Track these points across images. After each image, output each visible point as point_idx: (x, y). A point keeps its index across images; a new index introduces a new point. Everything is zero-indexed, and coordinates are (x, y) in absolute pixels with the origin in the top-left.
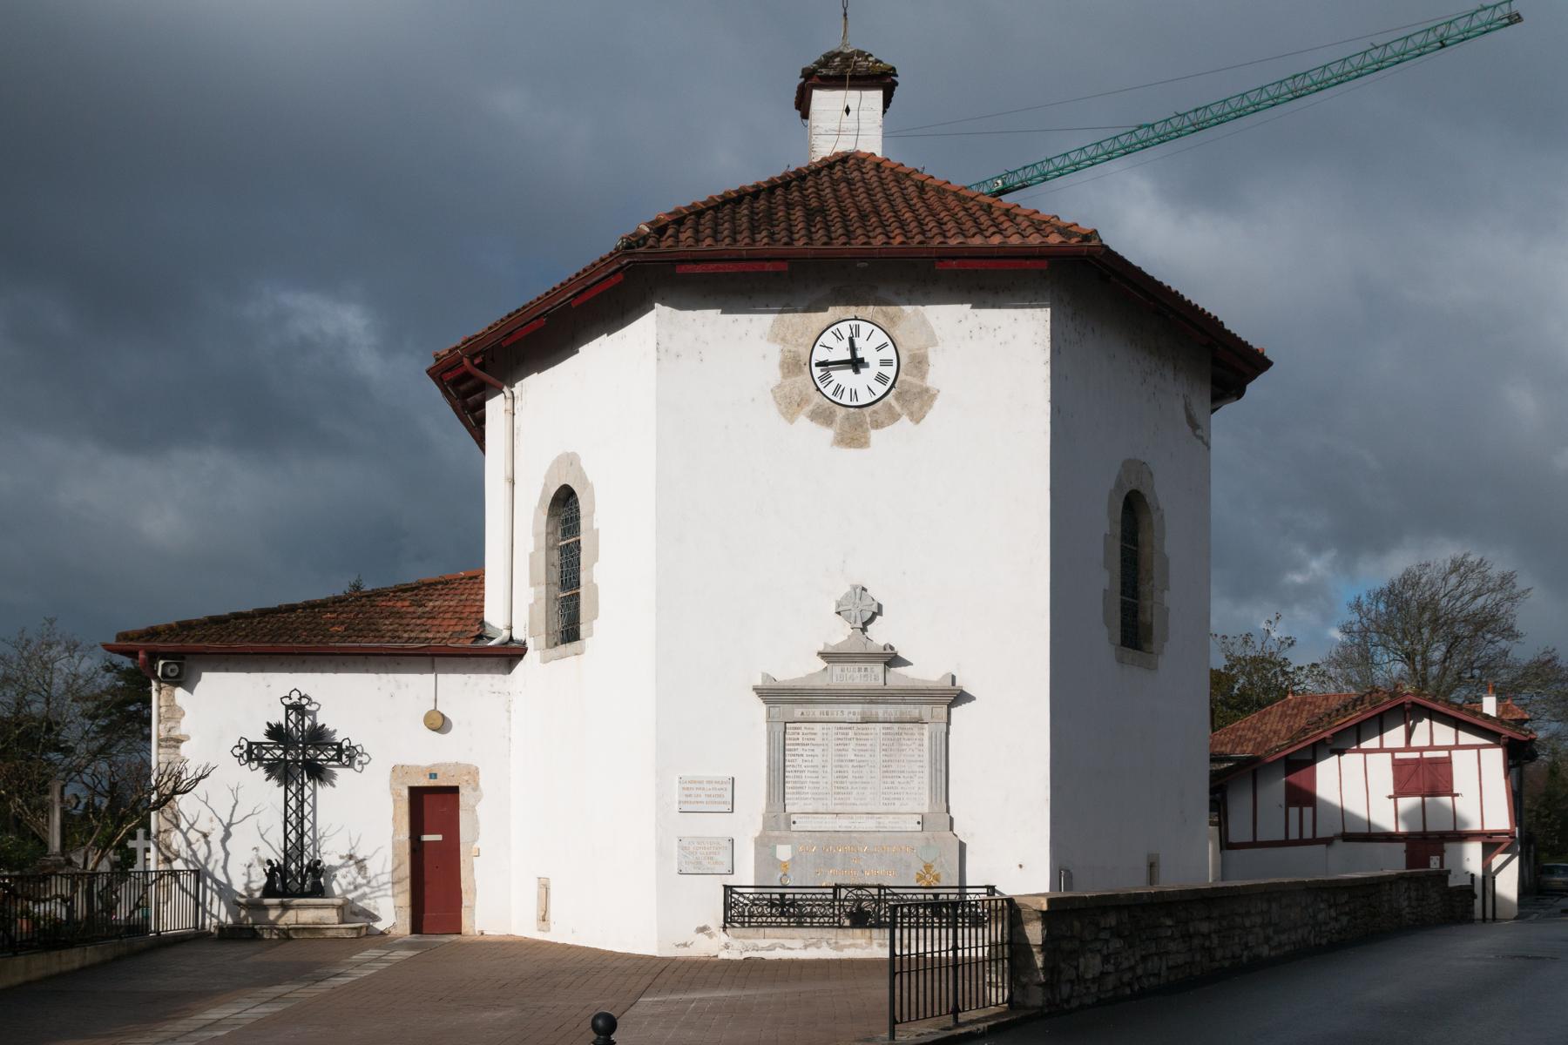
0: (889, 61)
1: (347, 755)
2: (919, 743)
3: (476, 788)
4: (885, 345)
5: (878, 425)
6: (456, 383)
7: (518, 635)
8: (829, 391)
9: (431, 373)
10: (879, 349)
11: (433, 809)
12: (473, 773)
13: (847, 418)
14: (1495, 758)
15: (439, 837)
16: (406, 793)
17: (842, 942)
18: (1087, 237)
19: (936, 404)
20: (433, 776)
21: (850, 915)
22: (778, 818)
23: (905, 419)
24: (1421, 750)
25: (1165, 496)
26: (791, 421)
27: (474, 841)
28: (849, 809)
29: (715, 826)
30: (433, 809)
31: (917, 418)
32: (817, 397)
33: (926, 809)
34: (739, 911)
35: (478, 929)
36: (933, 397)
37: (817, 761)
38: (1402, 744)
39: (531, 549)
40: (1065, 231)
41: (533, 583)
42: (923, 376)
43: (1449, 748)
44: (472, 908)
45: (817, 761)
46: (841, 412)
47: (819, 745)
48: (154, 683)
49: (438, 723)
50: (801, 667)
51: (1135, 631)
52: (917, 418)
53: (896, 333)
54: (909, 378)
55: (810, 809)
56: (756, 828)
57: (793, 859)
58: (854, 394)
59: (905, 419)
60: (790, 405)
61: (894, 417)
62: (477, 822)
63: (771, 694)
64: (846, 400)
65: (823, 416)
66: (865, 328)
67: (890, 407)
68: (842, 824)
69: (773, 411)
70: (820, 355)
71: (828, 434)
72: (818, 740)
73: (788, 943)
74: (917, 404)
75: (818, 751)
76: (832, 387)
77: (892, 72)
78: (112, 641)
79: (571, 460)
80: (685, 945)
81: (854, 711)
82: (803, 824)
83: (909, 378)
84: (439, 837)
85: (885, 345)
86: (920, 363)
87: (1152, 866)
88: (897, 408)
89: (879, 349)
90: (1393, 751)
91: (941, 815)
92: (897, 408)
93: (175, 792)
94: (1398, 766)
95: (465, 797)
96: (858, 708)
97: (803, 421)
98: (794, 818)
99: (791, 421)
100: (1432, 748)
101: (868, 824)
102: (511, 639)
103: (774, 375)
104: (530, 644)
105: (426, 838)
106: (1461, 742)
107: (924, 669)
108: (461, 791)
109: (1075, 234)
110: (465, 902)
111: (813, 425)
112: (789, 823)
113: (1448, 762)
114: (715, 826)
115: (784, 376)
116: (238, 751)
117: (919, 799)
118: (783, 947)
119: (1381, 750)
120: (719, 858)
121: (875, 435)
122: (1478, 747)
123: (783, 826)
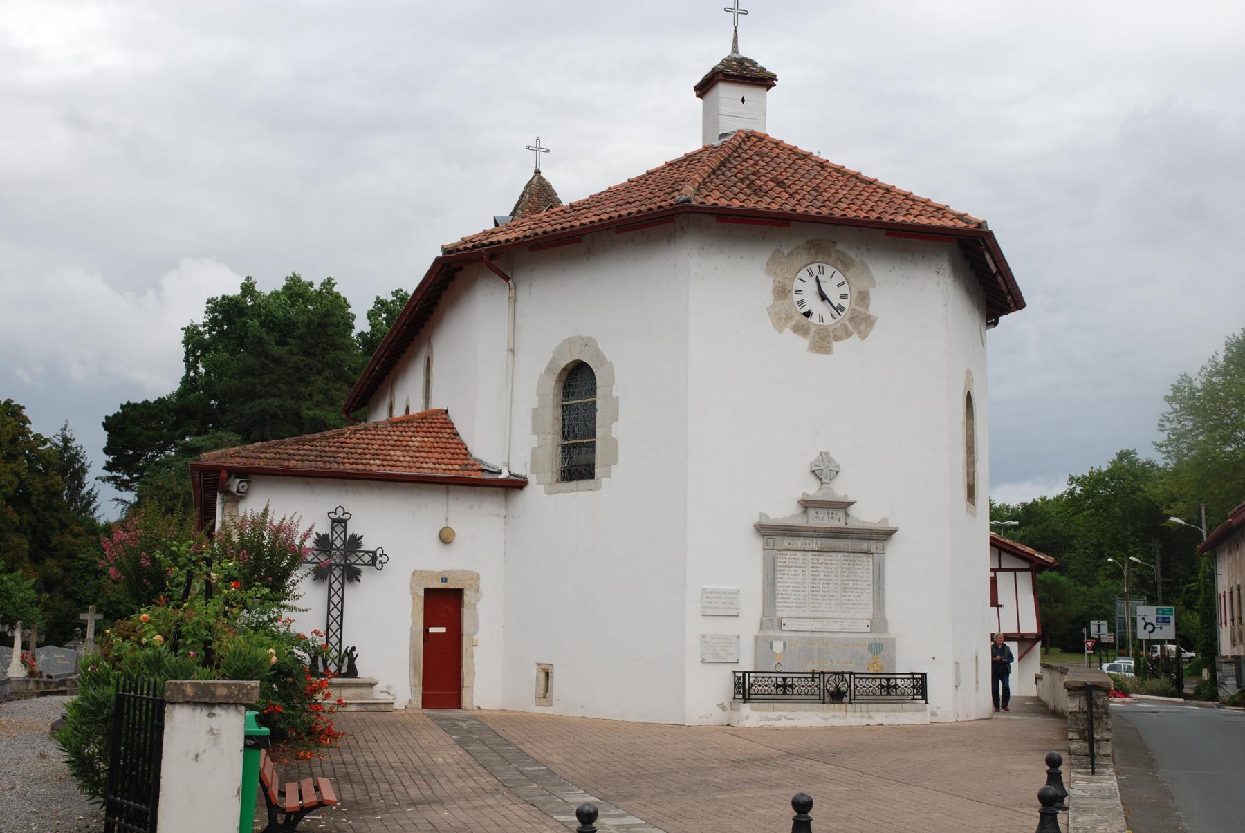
2: (864, 565)
3: (477, 590)
10: (839, 285)
11: (444, 604)
12: (475, 577)
14: (1025, 581)
15: (443, 630)
16: (422, 593)
18: (980, 225)
19: (875, 327)
20: (444, 580)
22: (771, 620)
23: (855, 335)
27: (475, 633)
28: (820, 615)
29: (725, 627)
30: (444, 604)
31: (863, 336)
34: (743, 689)
35: (476, 703)
36: (873, 322)
37: (799, 579)
39: (534, 402)
40: (962, 217)
41: (536, 430)
42: (867, 308)
44: (471, 687)
47: (799, 568)
48: (219, 496)
50: (784, 511)
52: (863, 336)
55: (794, 614)
56: (754, 629)
59: (855, 335)
61: (848, 334)
62: (477, 618)
63: (767, 531)
66: (829, 270)
68: (817, 625)
73: (790, 715)
74: (863, 327)
75: (799, 571)
81: (814, 544)
82: (790, 625)
84: (443, 630)
88: (850, 328)
89: (839, 285)
91: (878, 622)
95: (468, 597)
101: (835, 626)
104: (532, 479)
105: (432, 630)
107: (865, 515)
109: (795, 154)
111: (795, 335)
112: (781, 625)
114: (725, 627)
116: (384, 559)
117: (865, 611)
123: (776, 627)
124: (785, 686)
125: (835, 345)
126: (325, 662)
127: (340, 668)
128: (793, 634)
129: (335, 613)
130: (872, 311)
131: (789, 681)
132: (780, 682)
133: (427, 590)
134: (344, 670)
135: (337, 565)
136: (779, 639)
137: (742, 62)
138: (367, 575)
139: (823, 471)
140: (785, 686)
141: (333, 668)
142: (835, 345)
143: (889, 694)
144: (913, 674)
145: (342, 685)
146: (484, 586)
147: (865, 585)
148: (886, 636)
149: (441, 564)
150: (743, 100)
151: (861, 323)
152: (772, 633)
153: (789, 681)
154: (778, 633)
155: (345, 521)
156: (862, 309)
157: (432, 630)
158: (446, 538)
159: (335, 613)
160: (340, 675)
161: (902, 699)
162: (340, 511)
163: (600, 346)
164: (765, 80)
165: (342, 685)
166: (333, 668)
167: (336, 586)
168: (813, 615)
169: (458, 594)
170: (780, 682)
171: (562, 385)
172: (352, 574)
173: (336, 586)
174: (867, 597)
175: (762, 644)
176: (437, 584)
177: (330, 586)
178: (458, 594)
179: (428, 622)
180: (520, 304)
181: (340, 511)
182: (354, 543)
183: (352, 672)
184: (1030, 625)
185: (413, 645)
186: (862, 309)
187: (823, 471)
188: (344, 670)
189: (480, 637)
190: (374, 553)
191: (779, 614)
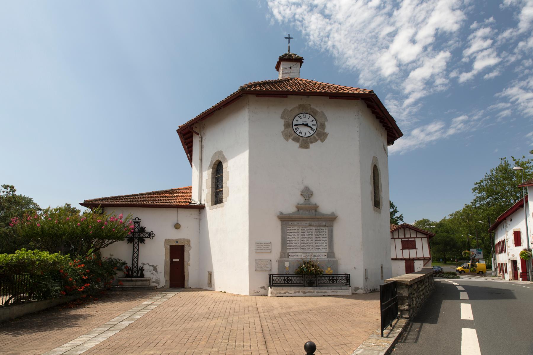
0: (301, 56)
1: (150, 235)
2: (326, 230)
3: (189, 246)
4: (313, 121)
5: (312, 142)
6: (184, 135)
7: (203, 203)
8: (298, 133)
9: (178, 131)
10: (312, 121)
12: (189, 241)
13: (303, 140)
14: (425, 241)
15: (178, 260)
16: (169, 247)
17: (306, 291)
19: (328, 137)
20: (177, 242)
21: (308, 283)
22: (284, 254)
23: (319, 141)
24: (408, 238)
25: (380, 167)
26: (287, 141)
29: (266, 257)
31: (323, 141)
32: (294, 134)
33: (327, 251)
37: (296, 237)
38: (403, 237)
43: (415, 238)
45: (296, 237)
46: (301, 139)
47: (295, 234)
49: (177, 226)
50: (290, 209)
51: (377, 204)
52: (323, 141)
53: (316, 117)
54: (320, 130)
57: (289, 266)
58: (305, 134)
59: (319, 141)
60: (287, 136)
61: (316, 141)
64: (303, 135)
65: (296, 139)
67: (315, 138)
69: (282, 138)
70: (295, 122)
71: (298, 145)
72: (296, 231)
74: (322, 137)
75: (296, 234)
76: (299, 131)
77: (302, 59)
78: (83, 202)
79: (220, 153)
80: (257, 292)
83: (320, 130)
84: (178, 260)
85: (313, 121)
86: (323, 126)
87: (382, 267)
88: (317, 138)
89: (312, 121)
90: (401, 238)
91: (331, 254)
92: (317, 138)
93: (101, 247)
94: (402, 241)
96: (308, 222)
97: (290, 141)
98: (289, 254)
99: (287, 141)
100: (411, 238)
102: (200, 204)
103: (282, 128)
104: (206, 205)
105: (174, 260)
106: (418, 236)
108: (185, 247)
110: (186, 279)
112: (288, 256)
113: (415, 241)
115: (285, 128)
116: (153, 235)
118: (288, 293)
119: (399, 238)
120: (268, 266)
121: (311, 145)
122: (422, 238)
124: (288, 280)
125: (311, 145)
126: (132, 272)
127: (138, 274)
128: (294, 259)
129: (136, 255)
130: (326, 131)
131: (290, 278)
132: (286, 278)
133: (170, 246)
134: (139, 275)
135: (136, 238)
136: (287, 261)
137: (290, 55)
138: (147, 240)
139: (307, 193)
140: (288, 280)
141: (135, 274)
142: (311, 145)
143: (333, 283)
144: (346, 274)
145: (137, 281)
146: (192, 244)
147: (324, 239)
148: (334, 259)
149: (175, 236)
150: (291, 68)
151: (320, 135)
152: (285, 259)
153: (290, 278)
154: (287, 259)
155: (139, 222)
156: (322, 130)
157: (174, 260)
158: (177, 226)
159: (136, 255)
160: (137, 277)
161: (341, 285)
162: (137, 219)
163: (224, 154)
164: (299, 61)
165: (137, 281)
166: (135, 274)
167: (136, 245)
168: (302, 251)
169: (182, 247)
170: (286, 278)
171: (215, 170)
172: (142, 241)
173: (136, 245)
174: (326, 244)
175: (281, 263)
176: (174, 244)
177: (134, 245)
178: (182, 247)
179: (171, 258)
180: (205, 143)
181: (137, 219)
182: (142, 230)
183: (142, 276)
184: (427, 255)
185: (166, 265)
186: (322, 130)
187: (307, 193)
188: (139, 275)
189: (191, 262)
190: (150, 233)
191: (288, 251)
